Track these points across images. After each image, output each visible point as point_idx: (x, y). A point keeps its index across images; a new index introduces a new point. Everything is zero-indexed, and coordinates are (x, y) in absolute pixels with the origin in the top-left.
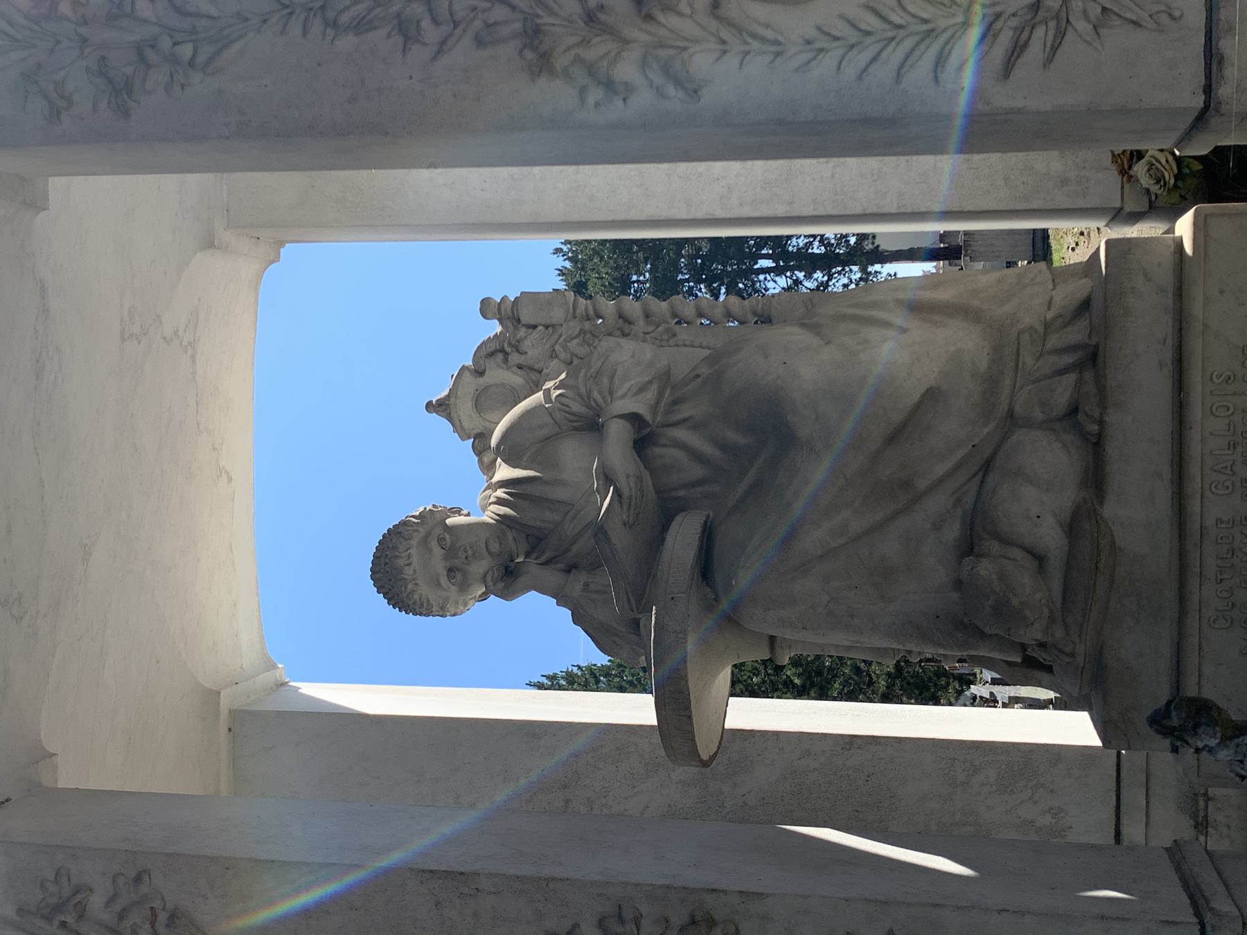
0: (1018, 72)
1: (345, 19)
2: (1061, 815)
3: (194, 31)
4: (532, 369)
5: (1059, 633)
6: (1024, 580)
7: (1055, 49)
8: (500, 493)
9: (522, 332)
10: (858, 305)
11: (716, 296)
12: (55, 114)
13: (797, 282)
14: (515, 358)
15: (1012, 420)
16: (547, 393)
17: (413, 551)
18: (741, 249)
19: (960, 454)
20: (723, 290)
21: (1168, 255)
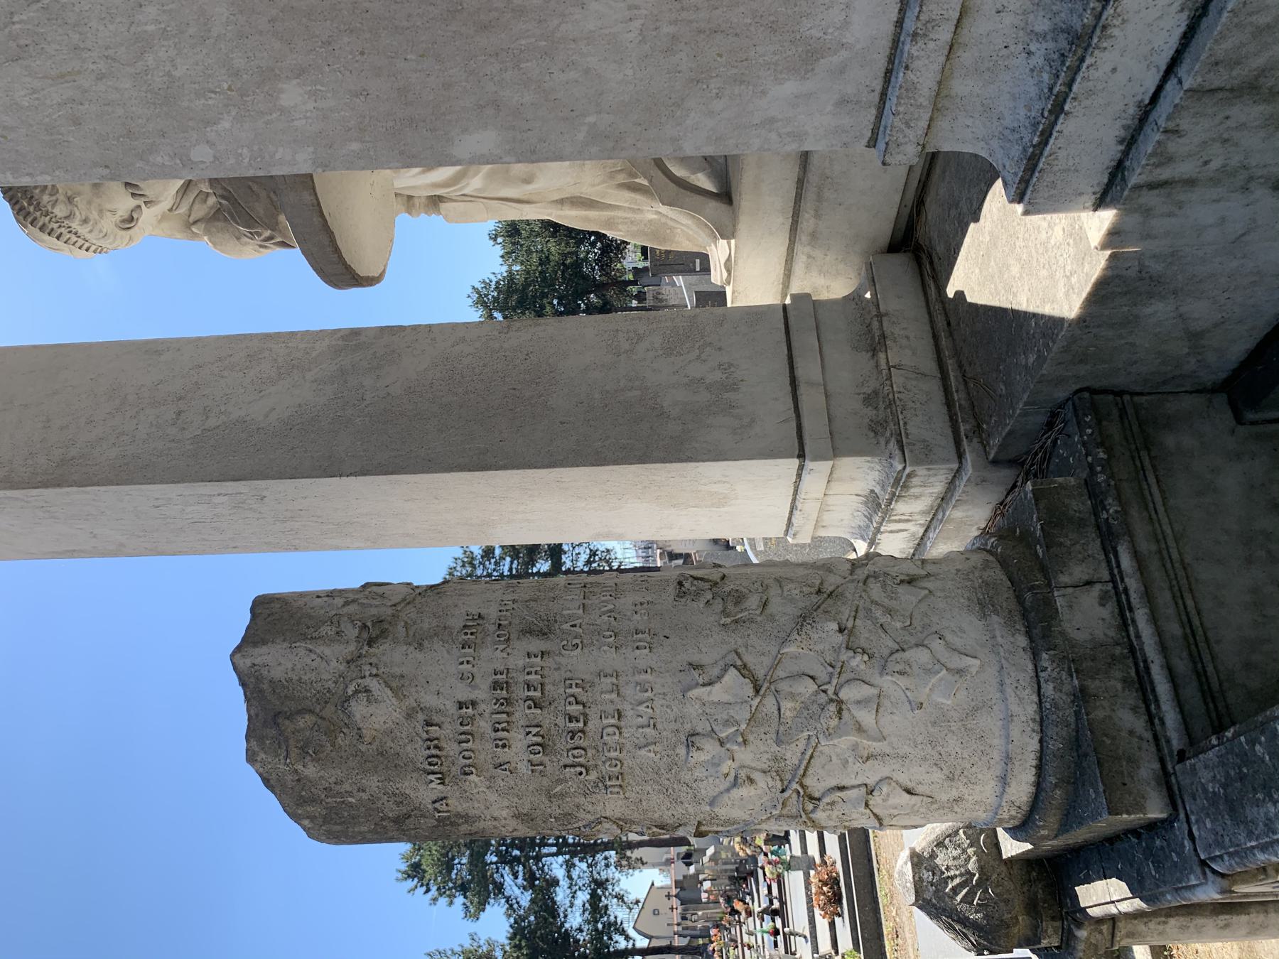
2: (732, 370)
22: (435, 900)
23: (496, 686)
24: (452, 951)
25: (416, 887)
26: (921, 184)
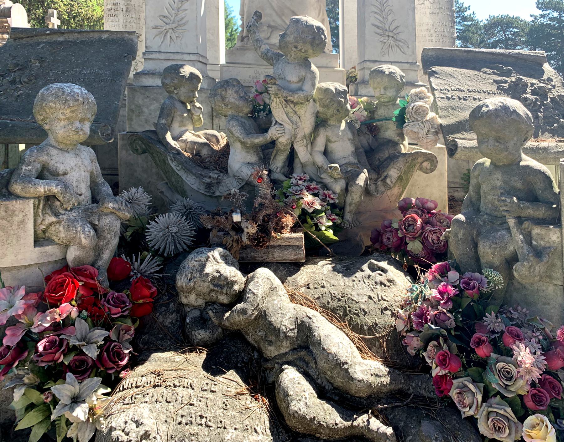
0: (373, 27)
7: (378, 34)
18: (353, 328)
21: (334, 66)
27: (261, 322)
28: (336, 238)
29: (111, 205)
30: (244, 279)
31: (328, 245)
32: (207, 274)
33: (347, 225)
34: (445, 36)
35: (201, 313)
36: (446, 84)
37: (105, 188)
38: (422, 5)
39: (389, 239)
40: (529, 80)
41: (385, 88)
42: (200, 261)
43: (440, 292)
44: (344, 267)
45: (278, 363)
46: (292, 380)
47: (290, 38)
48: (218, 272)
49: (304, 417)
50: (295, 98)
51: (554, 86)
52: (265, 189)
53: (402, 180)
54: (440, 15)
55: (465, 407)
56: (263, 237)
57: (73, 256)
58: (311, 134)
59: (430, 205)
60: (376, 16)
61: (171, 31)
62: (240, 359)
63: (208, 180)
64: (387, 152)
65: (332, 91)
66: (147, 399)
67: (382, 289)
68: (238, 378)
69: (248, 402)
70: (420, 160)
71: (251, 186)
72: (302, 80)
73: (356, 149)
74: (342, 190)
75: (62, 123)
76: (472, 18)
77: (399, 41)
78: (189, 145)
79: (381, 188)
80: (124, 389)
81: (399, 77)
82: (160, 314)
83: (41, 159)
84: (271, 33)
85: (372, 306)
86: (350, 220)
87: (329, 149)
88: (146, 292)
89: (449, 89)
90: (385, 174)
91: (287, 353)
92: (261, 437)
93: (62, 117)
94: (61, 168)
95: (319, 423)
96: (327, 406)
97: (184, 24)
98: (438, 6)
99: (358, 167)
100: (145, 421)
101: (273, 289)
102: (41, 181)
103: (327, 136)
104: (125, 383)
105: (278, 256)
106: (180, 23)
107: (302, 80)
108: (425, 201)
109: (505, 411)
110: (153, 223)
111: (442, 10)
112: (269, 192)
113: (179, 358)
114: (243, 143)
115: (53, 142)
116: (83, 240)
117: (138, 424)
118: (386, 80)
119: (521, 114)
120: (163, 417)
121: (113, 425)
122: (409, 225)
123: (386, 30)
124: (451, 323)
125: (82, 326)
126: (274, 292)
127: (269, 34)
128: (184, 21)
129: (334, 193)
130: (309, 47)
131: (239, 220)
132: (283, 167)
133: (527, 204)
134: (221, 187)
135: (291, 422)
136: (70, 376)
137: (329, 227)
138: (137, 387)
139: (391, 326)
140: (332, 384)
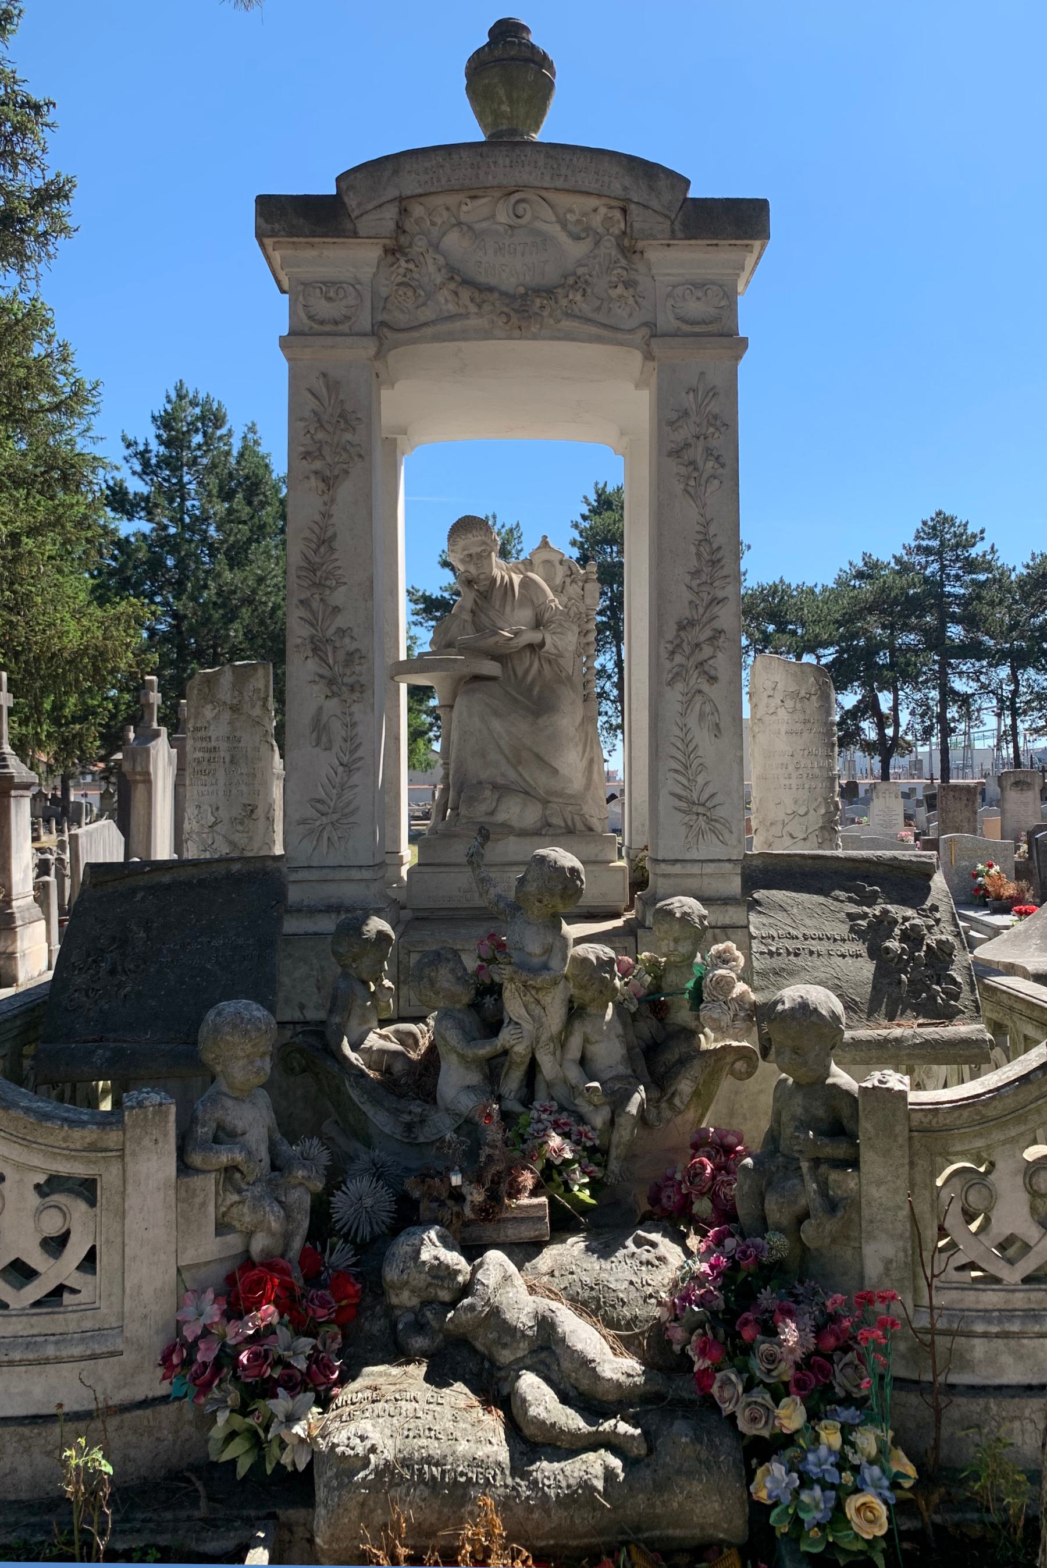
0: (672, 798)
1: (702, 549)
3: (700, 485)
4: (563, 588)
5: (464, 821)
6: (483, 808)
7: (680, 810)
8: (507, 578)
9: (580, 584)
10: (592, 742)
11: (600, 613)
12: (671, 424)
13: (609, 677)
14: (568, 580)
15: (545, 802)
16: (553, 601)
17: (479, 538)
19: (532, 783)
20: (604, 619)
21: (609, 858)
22: (576, 526)
23: (215, 748)
24: (521, 550)
25: (589, 505)
26: (425, 914)
27: (493, 1321)
28: (593, 1202)
29: (300, 1173)
30: (469, 1268)
31: (583, 1214)
32: (424, 1262)
33: (611, 1180)
34: (815, 777)
35: (416, 1315)
36: (771, 925)
37: (284, 1148)
38: (774, 717)
39: (669, 1197)
40: (897, 911)
41: (676, 941)
42: (413, 1245)
43: (712, 1267)
44: (601, 1244)
45: (514, 1370)
46: (531, 1385)
47: (532, 888)
48: (437, 1258)
49: (544, 1422)
50: (539, 982)
51: (938, 921)
52: (494, 1133)
53: (702, 1097)
54: (806, 735)
55: (725, 1403)
56: (492, 1207)
57: (261, 1246)
58: (560, 1033)
59: (731, 1139)
60: (676, 776)
61: (329, 828)
62: (467, 1370)
63: (407, 1118)
64: (677, 1050)
65: (592, 962)
66: (367, 1414)
67: (648, 1271)
68: (466, 1390)
69: (480, 1415)
70: (729, 1059)
71: (472, 1124)
72: (548, 951)
73: (630, 1049)
74: (604, 1123)
75: (241, 1063)
76: (989, 562)
77: (716, 821)
78: (375, 1057)
79: (667, 1114)
80: (337, 1408)
81: (697, 921)
82: (366, 1319)
83: (217, 1115)
84: (498, 800)
85: (634, 1294)
86: (617, 1171)
87: (589, 1055)
88: (351, 1290)
89: (775, 935)
90: (673, 1089)
91: (524, 1357)
92: (496, 1448)
93: (241, 1054)
94: (240, 1125)
95: (560, 1428)
96: (570, 1411)
97: (353, 813)
98: (802, 717)
99: (630, 1083)
100: (370, 1435)
101: (507, 1278)
102: (223, 1147)
103: (585, 1034)
104: (339, 1401)
105: (513, 1233)
106: (346, 811)
107: (548, 951)
108: (724, 1132)
109: (763, 1398)
110: (339, 1193)
111: (809, 726)
112: (500, 1136)
113: (395, 1371)
114: (462, 1057)
115: (225, 1088)
116: (273, 1224)
117: (362, 1438)
118: (677, 927)
119: (824, 1013)
120: (388, 1432)
121: (336, 1441)
122: (696, 1175)
123: (694, 803)
124: (720, 1303)
125: (284, 1334)
126: (509, 1282)
127: (494, 805)
128: (352, 807)
129: (594, 1129)
130: (559, 901)
131: (459, 1182)
132: (520, 1088)
133: (826, 1140)
134: (426, 1129)
135: (528, 1431)
136: (280, 1391)
137: (583, 1186)
138: (353, 1404)
139: (655, 1318)
140: (576, 1388)
